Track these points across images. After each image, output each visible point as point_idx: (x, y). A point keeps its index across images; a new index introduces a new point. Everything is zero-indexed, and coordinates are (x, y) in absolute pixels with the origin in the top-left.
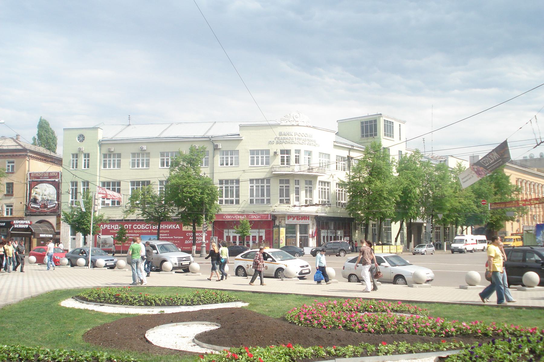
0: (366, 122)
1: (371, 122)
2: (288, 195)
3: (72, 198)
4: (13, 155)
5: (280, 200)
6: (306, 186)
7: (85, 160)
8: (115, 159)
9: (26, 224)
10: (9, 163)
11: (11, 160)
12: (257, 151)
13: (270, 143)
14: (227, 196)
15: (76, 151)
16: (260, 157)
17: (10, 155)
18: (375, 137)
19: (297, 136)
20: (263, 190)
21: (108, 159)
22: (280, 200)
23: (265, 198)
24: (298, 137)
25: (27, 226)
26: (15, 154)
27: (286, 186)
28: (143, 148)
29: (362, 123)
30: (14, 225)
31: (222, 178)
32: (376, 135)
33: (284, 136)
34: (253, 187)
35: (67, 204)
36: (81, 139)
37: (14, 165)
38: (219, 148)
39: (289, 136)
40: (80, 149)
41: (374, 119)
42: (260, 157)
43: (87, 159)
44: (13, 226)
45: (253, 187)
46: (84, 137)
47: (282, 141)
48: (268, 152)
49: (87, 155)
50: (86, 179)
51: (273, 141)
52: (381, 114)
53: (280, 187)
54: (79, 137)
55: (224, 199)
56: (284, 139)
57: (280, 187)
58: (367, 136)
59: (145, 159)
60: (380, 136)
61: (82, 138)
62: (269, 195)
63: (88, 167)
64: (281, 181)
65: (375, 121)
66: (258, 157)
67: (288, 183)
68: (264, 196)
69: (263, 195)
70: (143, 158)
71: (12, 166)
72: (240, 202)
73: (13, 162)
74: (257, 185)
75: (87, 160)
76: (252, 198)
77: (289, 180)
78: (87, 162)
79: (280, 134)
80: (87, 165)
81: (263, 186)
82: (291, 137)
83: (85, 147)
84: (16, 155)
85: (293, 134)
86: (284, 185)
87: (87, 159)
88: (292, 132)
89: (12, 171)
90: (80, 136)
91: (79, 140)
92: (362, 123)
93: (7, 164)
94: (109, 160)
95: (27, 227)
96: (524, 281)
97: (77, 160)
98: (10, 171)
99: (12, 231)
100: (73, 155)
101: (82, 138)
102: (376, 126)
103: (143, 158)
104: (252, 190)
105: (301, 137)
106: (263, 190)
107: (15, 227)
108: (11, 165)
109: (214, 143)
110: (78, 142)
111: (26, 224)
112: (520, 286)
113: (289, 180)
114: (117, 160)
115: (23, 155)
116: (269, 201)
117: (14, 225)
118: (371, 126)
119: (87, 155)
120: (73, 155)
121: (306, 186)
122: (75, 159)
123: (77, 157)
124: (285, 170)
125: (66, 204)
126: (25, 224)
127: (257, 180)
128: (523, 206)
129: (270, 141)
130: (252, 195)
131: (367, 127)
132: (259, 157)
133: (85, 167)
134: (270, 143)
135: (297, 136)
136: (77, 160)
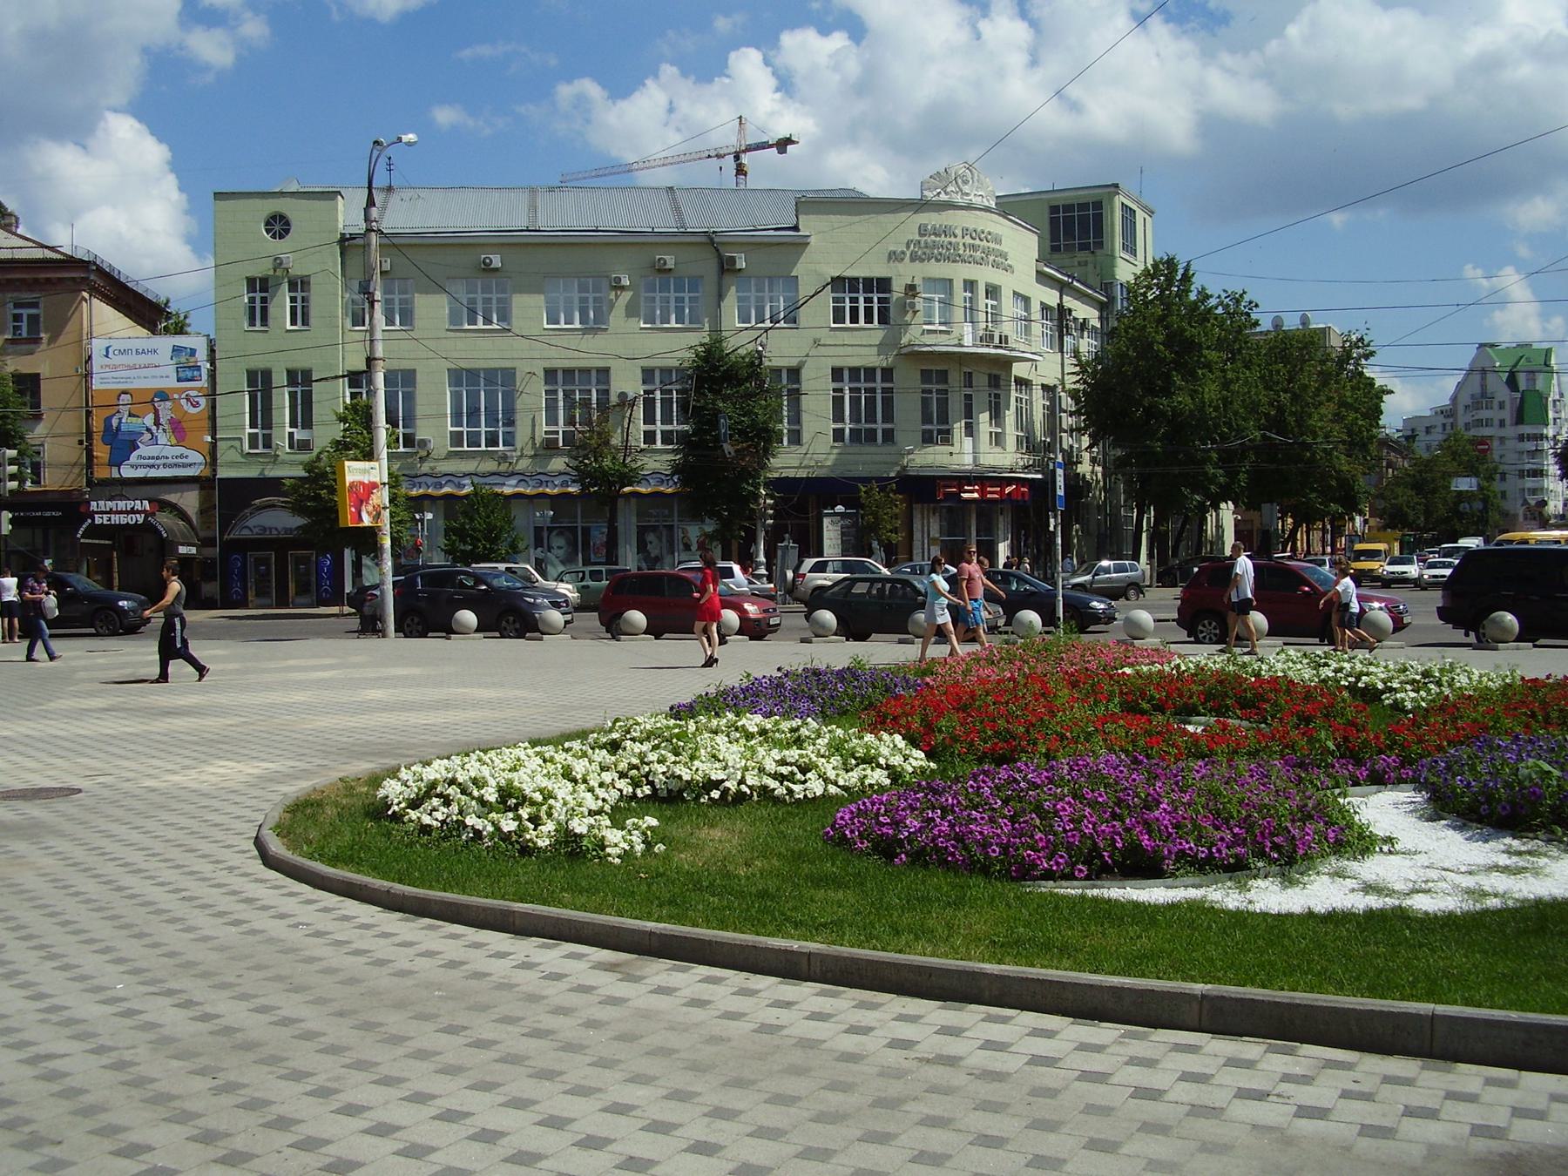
0: (1068, 208)
1: (1083, 206)
2: (944, 418)
3: (253, 425)
4: (36, 281)
5: (924, 432)
6: (927, 386)
7: (293, 300)
8: (682, 295)
9: (138, 512)
10: (17, 306)
11: (27, 296)
12: (853, 282)
13: (894, 257)
14: (855, 418)
15: (262, 269)
16: (861, 300)
17: (23, 281)
18: (1099, 252)
19: (968, 240)
20: (871, 402)
21: (672, 295)
22: (924, 432)
23: (880, 426)
24: (972, 242)
25: (140, 519)
26: (43, 276)
27: (938, 391)
28: (491, 261)
29: (1054, 209)
30: (92, 515)
31: (839, 363)
32: (1100, 245)
33: (933, 237)
34: (652, 392)
35: (237, 443)
36: (277, 228)
37: (38, 315)
38: (738, 267)
39: (948, 239)
40: (278, 263)
41: (1094, 200)
42: (861, 300)
43: (299, 295)
44: (90, 521)
45: (841, 390)
46: (288, 223)
47: (928, 251)
48: (884, 284)
49: (299, 284)
50: (300, 361)
51: (903, 253)
52: (1116, 186)
53: (834, 390)
54: (267, 223)
55: (659, 427)
56: (935, 245)
57: (923, 392)
58: (1069, 248)
59: (494, 296)
60: (1113, 250)
61: (279, 226)
62: (887, 416)
63: (305, 322)
64: (926, 376)
65: (1098, 205)
66: (854, 300)
67: (946, 381)
68: (654, 423)
69: (871, 418)
70: (583, 295)
71: (29, 316)
72: (806, 437)
73: (35, 305)
74: (853, 385)
75: (299, 300)
76: (650, 427)
77: (946, 371)
78: (299, 305)
79: (923, 231)
80: (301, 314)
81: (873, 390)
82: (953, 240)
83: (298, 253)
84: (48, 280)
85: (959, 232)
86: (934, 387)
87: (258, 296)
88: (956, 227)
89: (28, 333)
90: (274, 217)
91: (268, 231)
92: (1054, 209)
93: (11, 310)
94: (262, 298)
95: (141, 521)
96: (624, 628)
97: (264, 300)
98: (25, 335)
99: (82, 537)
100: (251, 282)
101: (279, 226)
102: (1099, 219)
103: (583, 295)
104: (838, 403)
105: (977, 242)
106: (871, 402)
107: (98, 521)
108: (25, 312)
109: (721, 251)
110: (268, 237)
111: (138, 512)
112: (537, 634)
113: (946, 371)
114: (497, 298)
115: (73, 279)
116: (889, 436)
117: (92, 515)
118: (1084, 221)
119: (299, 284)
120: (251, 282)
121: (927, 386)
122: (258, 296)
123: (264, 289)
124: (943, 344)
125: (233, 443)
126: (133, 511)
127: (855, 372)
128: (1062, 450)
129: (894, 253)
130: (838, 416)
131: (1069, 222)
132: (857, 298)
133: (294, 322)
134: (894, 257)
135: (968, 240)
136: (264, 300)
